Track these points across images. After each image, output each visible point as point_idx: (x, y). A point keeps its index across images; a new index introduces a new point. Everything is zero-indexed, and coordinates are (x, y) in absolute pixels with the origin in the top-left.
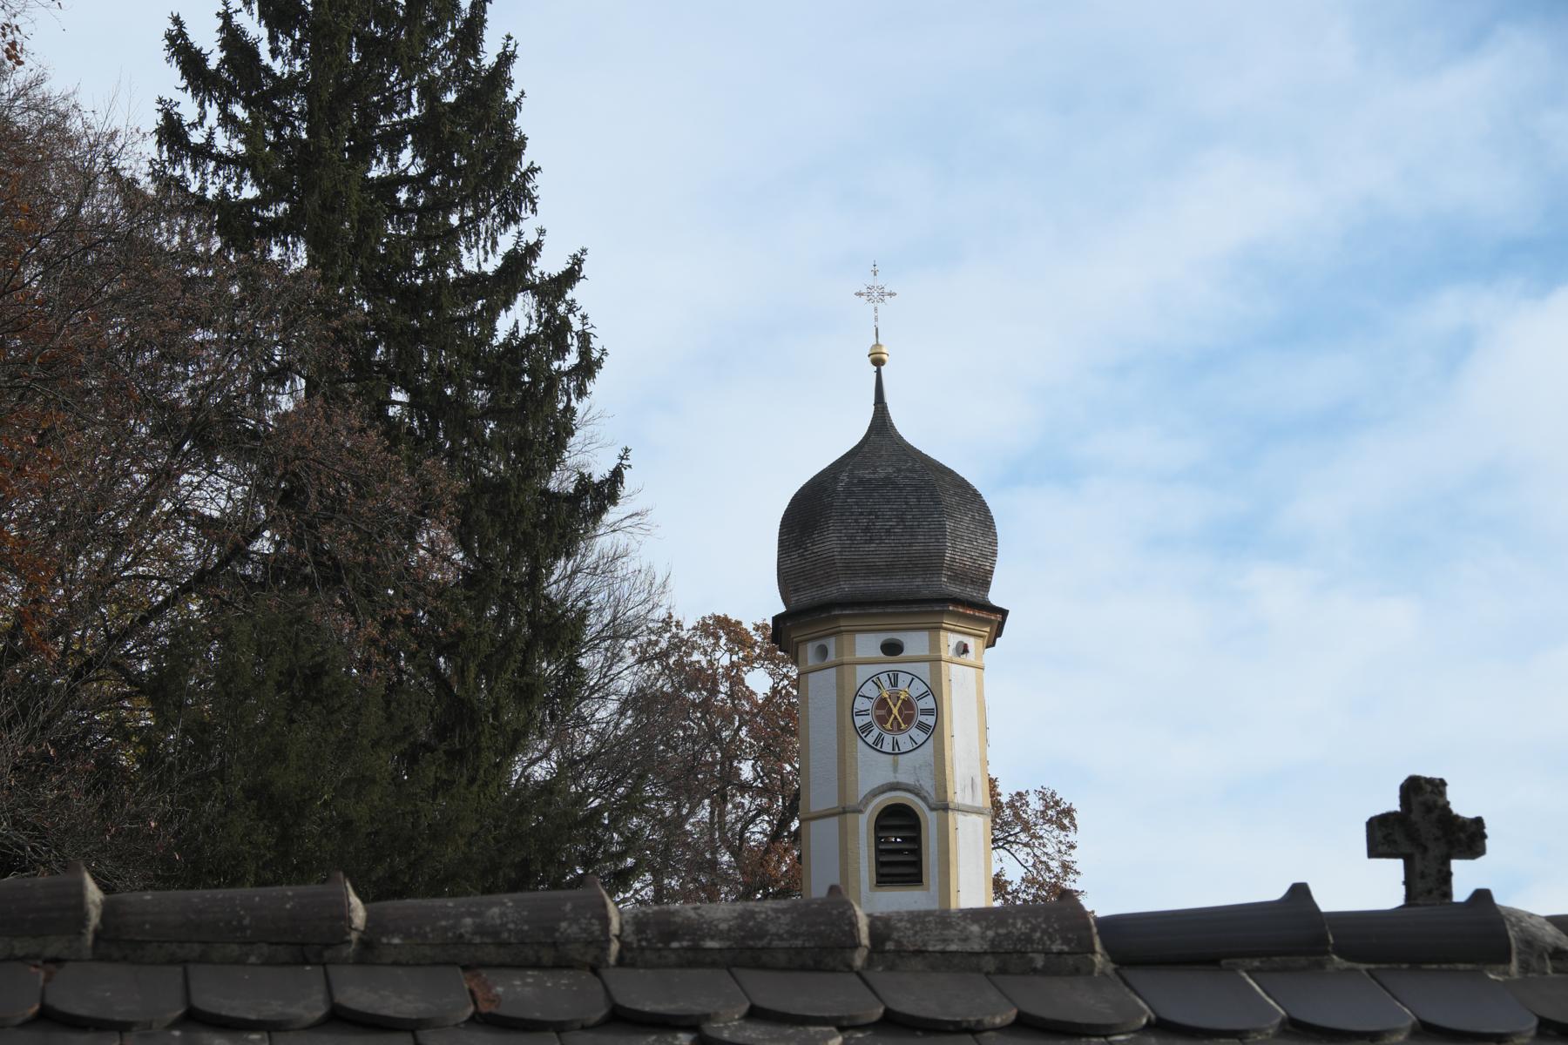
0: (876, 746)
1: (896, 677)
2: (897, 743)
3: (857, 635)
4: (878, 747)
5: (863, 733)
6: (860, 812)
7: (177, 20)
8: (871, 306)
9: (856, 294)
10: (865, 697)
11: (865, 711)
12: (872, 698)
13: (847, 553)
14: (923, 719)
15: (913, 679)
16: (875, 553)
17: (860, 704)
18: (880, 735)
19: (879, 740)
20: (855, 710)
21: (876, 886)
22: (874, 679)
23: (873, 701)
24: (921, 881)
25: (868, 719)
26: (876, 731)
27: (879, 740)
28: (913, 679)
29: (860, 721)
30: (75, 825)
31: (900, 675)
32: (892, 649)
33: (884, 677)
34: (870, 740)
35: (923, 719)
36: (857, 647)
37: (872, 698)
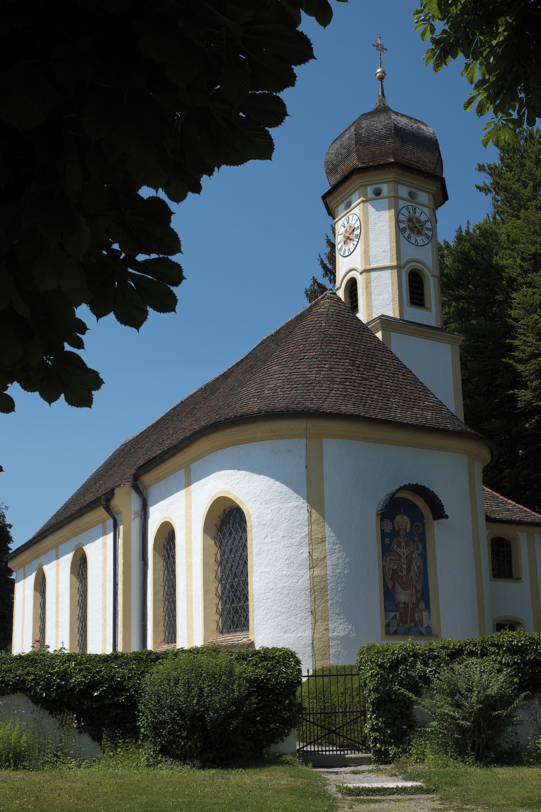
0: (408, 238)
1: (415, 209)
6: (403, 268)
8: (379, 52)
14: (427, 232)
17: (401, 218)
18: (409, 234)
19: (409, 236)
26: (408, 232)
27: (409, 236)
29: (402, 225)
32: (412, 195)
33: (410, 208)
34: (406, 235)
35: (427, 232)
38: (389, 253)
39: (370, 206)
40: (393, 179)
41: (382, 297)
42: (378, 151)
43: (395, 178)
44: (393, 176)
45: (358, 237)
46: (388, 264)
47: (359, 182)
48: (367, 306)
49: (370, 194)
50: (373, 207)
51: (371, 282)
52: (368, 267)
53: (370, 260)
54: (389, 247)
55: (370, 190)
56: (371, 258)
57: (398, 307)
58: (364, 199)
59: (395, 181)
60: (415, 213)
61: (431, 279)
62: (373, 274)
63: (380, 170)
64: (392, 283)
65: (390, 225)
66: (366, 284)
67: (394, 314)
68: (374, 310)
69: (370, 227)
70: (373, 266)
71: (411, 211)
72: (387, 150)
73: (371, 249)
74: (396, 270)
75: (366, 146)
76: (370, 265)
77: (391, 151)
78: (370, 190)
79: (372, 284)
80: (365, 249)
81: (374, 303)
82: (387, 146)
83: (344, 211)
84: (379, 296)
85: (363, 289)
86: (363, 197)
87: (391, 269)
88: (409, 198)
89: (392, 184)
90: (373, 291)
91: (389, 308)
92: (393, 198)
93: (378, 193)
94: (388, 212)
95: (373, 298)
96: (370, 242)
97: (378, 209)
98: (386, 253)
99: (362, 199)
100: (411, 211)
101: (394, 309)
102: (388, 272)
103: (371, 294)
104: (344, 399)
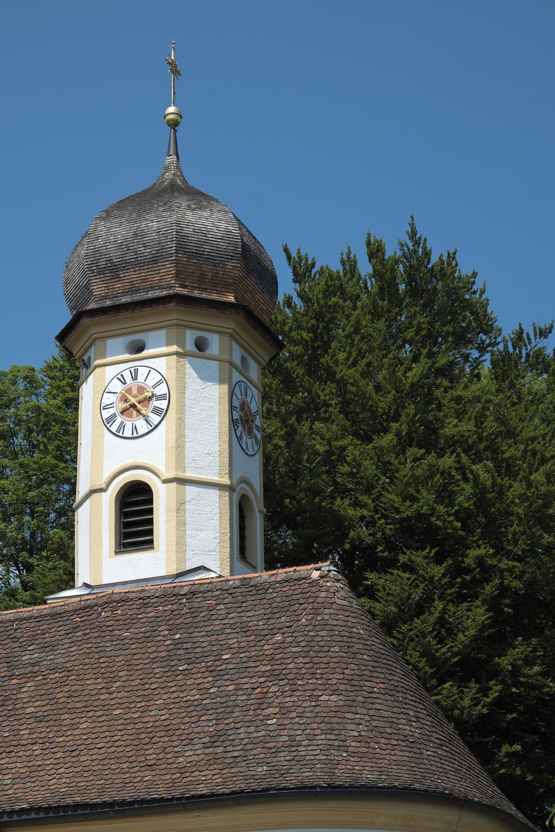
1: (136, 371)
2: (136, 428)
3: (108, 341)
4: (120, 434)
5: (108, 423)
7: (551, 327)
9: (534, 324)
10: (110, 392)
11: (111, 404)
12: (117, 393)
13: (163, 271)
15: (150, 371)
16: (152, 269)
17: (108, 399)
18: (122, 422)
19: (122, 426)
20: (103, 405)
21: (117, 553)
22: (119, 376)
23: (117, 395)
24: (151, 542)
25: (111, 411)
26: (119, 419)
27: (122, 426)
28: (150, 371)
30: (358, 322)
31: (123, 373)
34: (114, 428)
36: (107, 348)
37: (117, 393)
38: (218, 459)
39: (188, 366)
40: (231, 331)
41: (202, 535)
42: (211, 274)
43: (233, 329)
44: (232, 327)
45: (162, 413)
46: (216, 478)
47: (175, 317)
48: (177, 543)
49: (190, 346)
50: (195, 368)
51: (184, 503)
52: (181, 475)
53: (184, 463)
54: (217, 448)
55: (190, 336)
56: (186, 459)
57: (228, 560)
58: (181, 350)
59: (231, 335)
60: (135, 378)
61: (258, 514)
62: (190, 490)
63: (216, 311)
64: (221, 514)
65: (220, 410)
66: (177, 505)
67: (222, 570)
68: (189, 554)
69: (187, 403)
70: (189, 474)
71: (128, 379)
72: (226, 276)
73: (187, 444)
74: (227, 494)
75: (193, 259)
76: (184, 471)
77: (232, 281)
78: (190, 336)
79: (188, 506)
80: (177, 440)
81: (189, 541)
82: (227, 270)
83: (123, 354)
84: (198, 532)
85: (168, 511)
86: (179, 346)
87: (220, 490)
88: (197, 350)
89: (227, 338)
90: (188, 520)
91: (214, 557)
92: (228, 363)
93: (201, 345)
94: (217, 386)
95: (188, 532)
96: (186, 431)
97: (204, 377)
98: (212, 458)
99: (174, 348)
100: (128, 379)
101: (221, 560)
102: (215, 493)
103: (184, 524)
104: (460, 780)
